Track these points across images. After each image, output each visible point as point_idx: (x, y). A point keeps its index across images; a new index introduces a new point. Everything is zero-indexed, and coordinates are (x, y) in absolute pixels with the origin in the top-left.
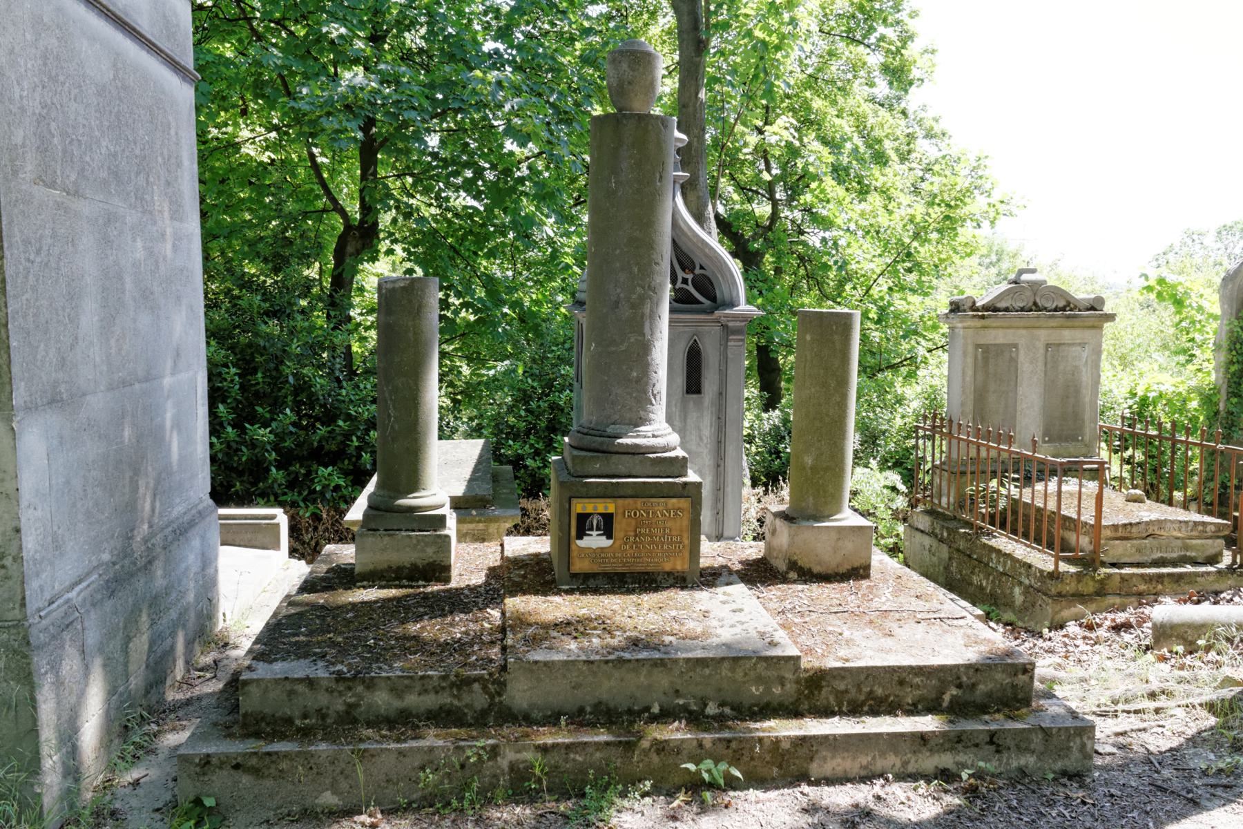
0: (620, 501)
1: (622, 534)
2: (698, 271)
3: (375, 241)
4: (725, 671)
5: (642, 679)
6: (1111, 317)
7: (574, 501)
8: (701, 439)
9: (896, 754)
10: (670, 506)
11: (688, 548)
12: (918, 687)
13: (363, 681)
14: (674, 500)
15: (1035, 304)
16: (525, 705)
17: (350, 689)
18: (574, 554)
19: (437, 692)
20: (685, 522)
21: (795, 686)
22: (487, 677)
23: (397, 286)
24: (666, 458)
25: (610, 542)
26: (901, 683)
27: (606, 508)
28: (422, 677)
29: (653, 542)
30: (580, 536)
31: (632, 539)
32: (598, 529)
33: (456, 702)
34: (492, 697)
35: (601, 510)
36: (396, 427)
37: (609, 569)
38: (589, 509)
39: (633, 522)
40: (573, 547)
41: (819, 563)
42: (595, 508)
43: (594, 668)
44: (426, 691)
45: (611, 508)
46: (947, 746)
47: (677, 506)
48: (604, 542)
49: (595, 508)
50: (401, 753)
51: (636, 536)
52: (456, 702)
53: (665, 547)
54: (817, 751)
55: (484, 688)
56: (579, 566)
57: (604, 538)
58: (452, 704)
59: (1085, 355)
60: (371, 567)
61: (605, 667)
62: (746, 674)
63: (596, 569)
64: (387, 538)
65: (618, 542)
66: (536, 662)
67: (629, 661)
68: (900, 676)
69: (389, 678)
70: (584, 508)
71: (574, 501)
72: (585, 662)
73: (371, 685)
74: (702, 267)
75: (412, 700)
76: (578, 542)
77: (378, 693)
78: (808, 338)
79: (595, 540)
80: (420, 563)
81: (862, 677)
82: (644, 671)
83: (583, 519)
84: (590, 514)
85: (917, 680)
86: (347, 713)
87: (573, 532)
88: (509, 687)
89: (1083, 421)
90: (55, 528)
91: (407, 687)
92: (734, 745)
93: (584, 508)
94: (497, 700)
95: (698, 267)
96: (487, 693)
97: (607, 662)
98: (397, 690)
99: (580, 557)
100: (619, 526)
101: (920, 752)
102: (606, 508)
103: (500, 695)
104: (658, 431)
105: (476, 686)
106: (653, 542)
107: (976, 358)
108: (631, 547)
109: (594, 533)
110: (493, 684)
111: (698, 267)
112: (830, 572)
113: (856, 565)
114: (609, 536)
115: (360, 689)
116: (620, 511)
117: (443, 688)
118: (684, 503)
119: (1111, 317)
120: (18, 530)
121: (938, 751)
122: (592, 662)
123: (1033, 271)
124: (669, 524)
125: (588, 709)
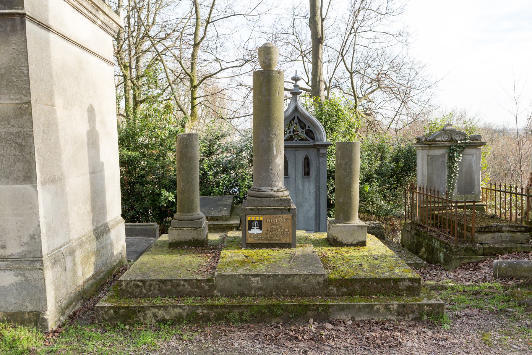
0: (265, 216)
1: (266, 228)
2: (307, 128)
6: (484, 144)
7: (247, 216)
10: (284, 217)
14: (285, 215)
15: (452, 139)
18: (248, 236)
25: (261, 231)
27: (259, 218)
29: (278, 231)
30: (250, 229)
32: (257, 226)
35: (257, 219)
37: (261, 242)
38: (253, 219)
40: (247, 233)
42: (255, 218)
45: (261, 218)
48: (259, 232)
49: (255, 218)
56: (250, 240)
59: (474, 159)
63: (256, 242)
65: (264, 232)
70: (251, 218)
74: (309, 127)
76: (249, 231)
79: (255, 231)
83: (251, 222)
87: (247, 228)
89: (474, 186)
90: (54, 225)
93: (251, 218)
99: (250, 237)
100: (264, 226)
102: (259, 218)
104: (279, 187)
106: (278, 231)
107: (428, 161)
109: (255, 228)
114: (261, 229)
116: (265, 219)
118: (290, 216)
119: (484, 144)
120: (39, 226)
123: (451, 125)
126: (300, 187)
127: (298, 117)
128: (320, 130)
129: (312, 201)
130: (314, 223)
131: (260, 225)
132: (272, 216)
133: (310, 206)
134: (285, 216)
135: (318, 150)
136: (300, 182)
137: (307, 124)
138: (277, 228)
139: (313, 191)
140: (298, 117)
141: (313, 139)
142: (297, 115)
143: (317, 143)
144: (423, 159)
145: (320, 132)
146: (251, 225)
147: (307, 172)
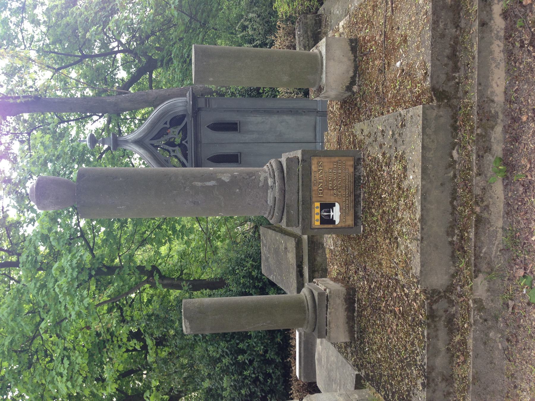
0: (314, 199)
1: (332, 197)
3: (134, 75)
4: (430, 155)
5: (433, 207)
8: (263, 122)
9: (491, 43)
10: (316, 170)
11: (341, 158)
12: (446, 25)
13: (429, 373)
14: (313, 167)
16: (446, 277)
17: (433, 380)
18: (343, 225)
19: (437, 330)
20: (325, 160)
21: (442, 109)
22: (429, 301)
23: (189, 327)
24: (287, 172)
25: (337, 204)
26: (443, 36)
28: (428, 339)
30: (333, 222)
31: (335, 192)
33: (443, 319)
34: (441, 297)
35: (318, 211)
36: (269, 322)
37: (352, 205)
38: (318, 217)
39: (325, 191)
40: (340, 225)
41: (348, 72)
42: (317, 214)
43: (425, 237)
44: (436, 336)
45: (317, 204)
46: (488, 9)
47: (316, 165)
49: (317, 214)
50: (476, 356)
51: (333, 189)
52: (443, 319)
53: (340, 171)
54: (487, 98)
55: (436, 302)
56: (350, 221)
57: (334, 208)
58: (444, 321)
60: (347, 333)
61: (425, 230)
62: (433, 141)
63: (352, 212)
64: (331, 325)
65: (337, 199)
66: (421, 271)
67: (422, 215)
68: (438, 36)
69: (428, 358)
70: (317, 220)
71: (313, 226)
72: (422, 242)
73: (431, 368)
74: (166, 123)
75: (441, 345)
76: (337, 223)
77: (436, 364)
78: (211, 79)
79: (336, 213)
80: (344, 307)
81: (438, 63)
82: (429, 206)
84: (321, 217)
85: (441, 25)
86: (447, 380)
87: (331, 226)
88: (436, 288)
91: (433, 347)
92: (481, 153)
93: (317, 220)
94: (442, 294)
95: (166, 126)
96: (439, 301)
97: (422, 229)
98: (433, 353)
100: (328, 200)
101: (491, 27)
103: (440, 292)
105: (434, 307)
106: (337, 179)
108: (340, 192)
109: (332, 214)
110: (433, 297)
111: (166, 126)
112: (353, 65)
113: (349, 48)
114: (334, 205)
115: (433, 374)
116: (319, 199)
117: (435, 326)
118: (315, 161)
121: (491, 15)
122: (422, 238)
124: (326, 169)
125: (450, 239)
126: (255, 136)
127: (151, 140)
128: (170, 106)
129: (274, 119)
130: (304, 117)
131: (327, 207)
132: (314, 188)
133: (281, 122)
134: (314, 168)
135: (199, 109)
136: (247, 138)
137: (161, 126)
138: (332, 180)
139: (259, 119)
140: (151, 140)
141: (183, 117)
142: (147, 141)
143: (190, 112)
144: (308, 309)
145: (174, 106)
146: (327, 221)
147: (232, 127)
